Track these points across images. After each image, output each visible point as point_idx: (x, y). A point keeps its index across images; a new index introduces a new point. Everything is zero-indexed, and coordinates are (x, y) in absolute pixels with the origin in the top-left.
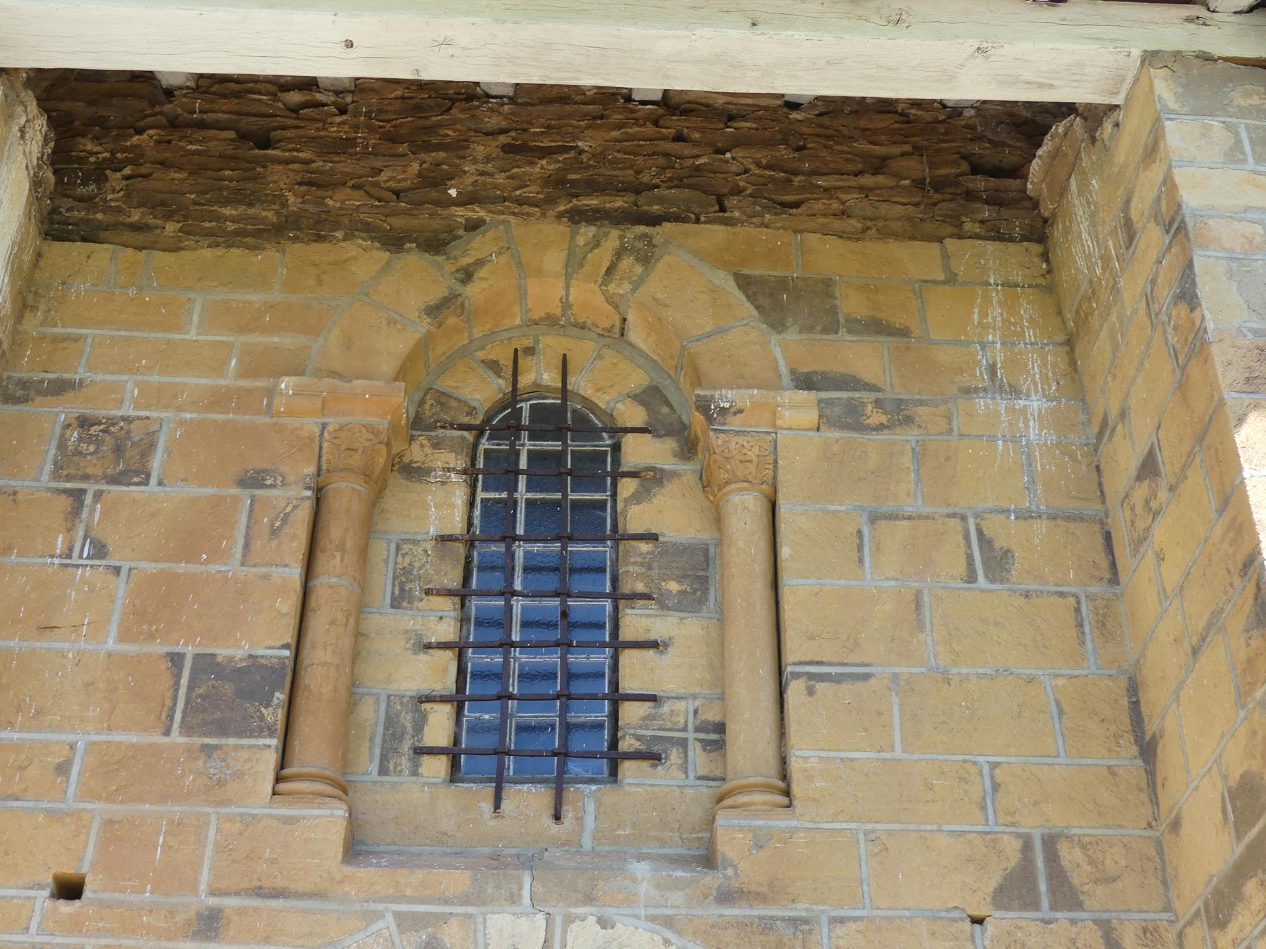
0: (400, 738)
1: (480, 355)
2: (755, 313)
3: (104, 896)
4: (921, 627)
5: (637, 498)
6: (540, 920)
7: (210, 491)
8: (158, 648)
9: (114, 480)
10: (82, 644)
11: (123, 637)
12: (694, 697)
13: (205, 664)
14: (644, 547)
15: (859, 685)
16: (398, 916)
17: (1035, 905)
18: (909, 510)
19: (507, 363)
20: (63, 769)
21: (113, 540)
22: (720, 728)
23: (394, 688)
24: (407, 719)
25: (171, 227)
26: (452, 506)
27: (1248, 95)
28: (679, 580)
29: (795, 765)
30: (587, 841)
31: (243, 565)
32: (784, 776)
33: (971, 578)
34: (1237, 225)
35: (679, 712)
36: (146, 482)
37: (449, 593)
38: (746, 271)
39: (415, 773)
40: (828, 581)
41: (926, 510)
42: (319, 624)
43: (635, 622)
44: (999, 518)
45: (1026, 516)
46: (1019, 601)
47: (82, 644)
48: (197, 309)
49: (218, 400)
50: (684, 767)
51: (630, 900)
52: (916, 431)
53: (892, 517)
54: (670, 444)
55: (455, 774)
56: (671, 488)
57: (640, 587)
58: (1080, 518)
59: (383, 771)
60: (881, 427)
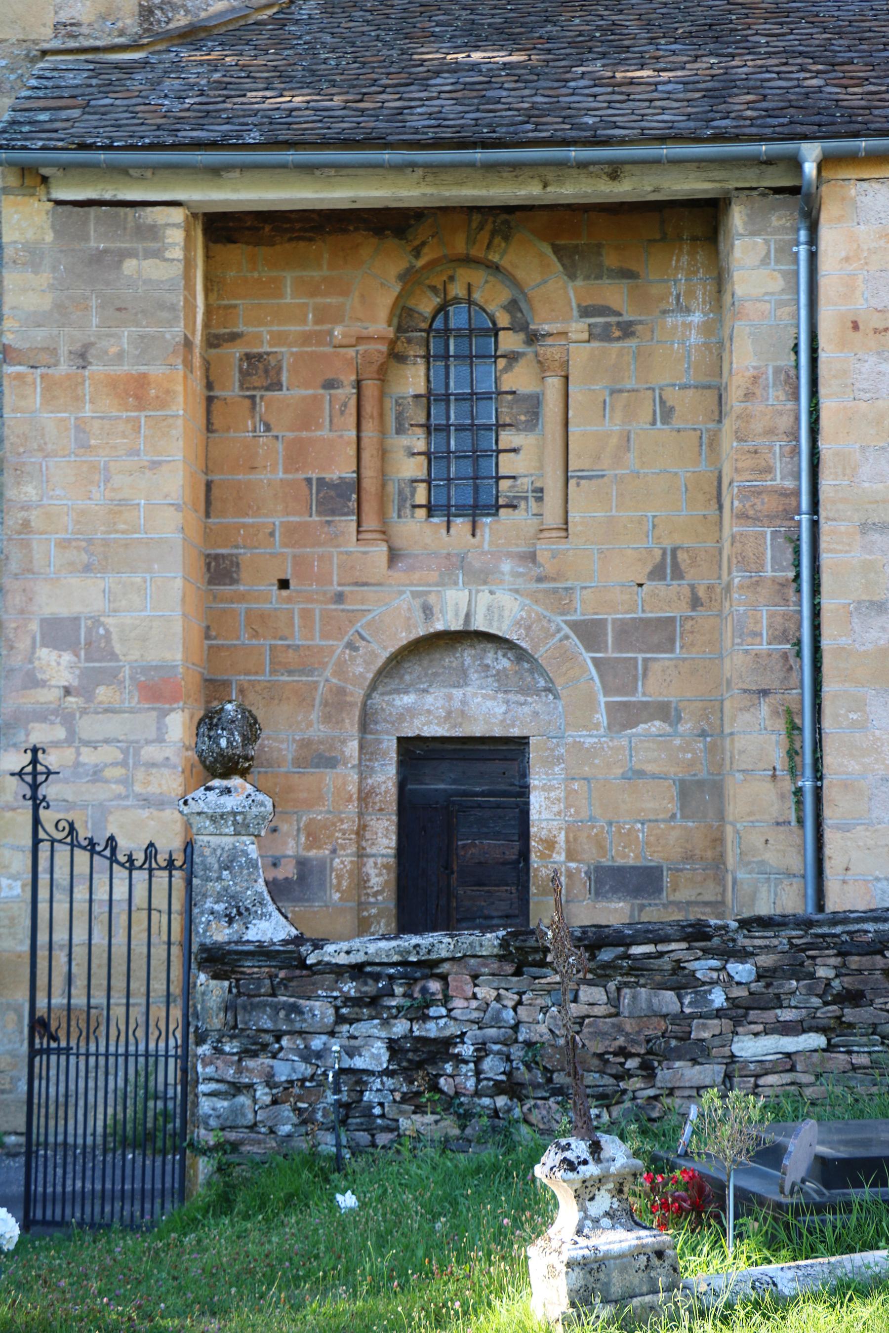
0: (405, 501)
1: (427, 282)
2: (561, 269)
3: (299, 588)
4: (629, 450)
5: (506, 369)
6: (467, 592)
7: (310, 392)
8: (301, 476)
9: (267, 389)
10: (269, 476)
11: (286, 471)
12: (532, 475)
13: (320, 481)
14: (510, 397)
15: (600, 481)
16: (412, 592)
17: (664, 579)
18: (629, 387)
19: (440, 287)
20: (272, 534)
21: (272, 422)
22: (541, 490)
23: (400, 476)
24: (407, 491)
25: (267, 228)
26: (419, 376)
27: (780, 218)
28: (525, 414)
29: (570, 519)
30: (486, 547)
31: (331, 430)
32: (566, 523)
33: (654, 423)
34: (758, 305)
35: (525, 483)
36: (281, 389)
37: (421, 426)
38: (558, 242)
39: (413, 517)
40: (588, 428)
41: (636, 387)
42: (366, 455)
43: (507, 438)
44: (670, 389)
45: (684, 387)
46: (674, 433)
47: (269, 476)
48: (289, 283)
49: (307, 339)
50: (527, 510)
51: (502, 582)
52: (636, 340)
53: (621, 391)
54: (522, 336)
55: (430, 515)
56: (522, 362)
57: (508, 421)
58: (709, 387)
59: (399, 516)
60: (619, 339)
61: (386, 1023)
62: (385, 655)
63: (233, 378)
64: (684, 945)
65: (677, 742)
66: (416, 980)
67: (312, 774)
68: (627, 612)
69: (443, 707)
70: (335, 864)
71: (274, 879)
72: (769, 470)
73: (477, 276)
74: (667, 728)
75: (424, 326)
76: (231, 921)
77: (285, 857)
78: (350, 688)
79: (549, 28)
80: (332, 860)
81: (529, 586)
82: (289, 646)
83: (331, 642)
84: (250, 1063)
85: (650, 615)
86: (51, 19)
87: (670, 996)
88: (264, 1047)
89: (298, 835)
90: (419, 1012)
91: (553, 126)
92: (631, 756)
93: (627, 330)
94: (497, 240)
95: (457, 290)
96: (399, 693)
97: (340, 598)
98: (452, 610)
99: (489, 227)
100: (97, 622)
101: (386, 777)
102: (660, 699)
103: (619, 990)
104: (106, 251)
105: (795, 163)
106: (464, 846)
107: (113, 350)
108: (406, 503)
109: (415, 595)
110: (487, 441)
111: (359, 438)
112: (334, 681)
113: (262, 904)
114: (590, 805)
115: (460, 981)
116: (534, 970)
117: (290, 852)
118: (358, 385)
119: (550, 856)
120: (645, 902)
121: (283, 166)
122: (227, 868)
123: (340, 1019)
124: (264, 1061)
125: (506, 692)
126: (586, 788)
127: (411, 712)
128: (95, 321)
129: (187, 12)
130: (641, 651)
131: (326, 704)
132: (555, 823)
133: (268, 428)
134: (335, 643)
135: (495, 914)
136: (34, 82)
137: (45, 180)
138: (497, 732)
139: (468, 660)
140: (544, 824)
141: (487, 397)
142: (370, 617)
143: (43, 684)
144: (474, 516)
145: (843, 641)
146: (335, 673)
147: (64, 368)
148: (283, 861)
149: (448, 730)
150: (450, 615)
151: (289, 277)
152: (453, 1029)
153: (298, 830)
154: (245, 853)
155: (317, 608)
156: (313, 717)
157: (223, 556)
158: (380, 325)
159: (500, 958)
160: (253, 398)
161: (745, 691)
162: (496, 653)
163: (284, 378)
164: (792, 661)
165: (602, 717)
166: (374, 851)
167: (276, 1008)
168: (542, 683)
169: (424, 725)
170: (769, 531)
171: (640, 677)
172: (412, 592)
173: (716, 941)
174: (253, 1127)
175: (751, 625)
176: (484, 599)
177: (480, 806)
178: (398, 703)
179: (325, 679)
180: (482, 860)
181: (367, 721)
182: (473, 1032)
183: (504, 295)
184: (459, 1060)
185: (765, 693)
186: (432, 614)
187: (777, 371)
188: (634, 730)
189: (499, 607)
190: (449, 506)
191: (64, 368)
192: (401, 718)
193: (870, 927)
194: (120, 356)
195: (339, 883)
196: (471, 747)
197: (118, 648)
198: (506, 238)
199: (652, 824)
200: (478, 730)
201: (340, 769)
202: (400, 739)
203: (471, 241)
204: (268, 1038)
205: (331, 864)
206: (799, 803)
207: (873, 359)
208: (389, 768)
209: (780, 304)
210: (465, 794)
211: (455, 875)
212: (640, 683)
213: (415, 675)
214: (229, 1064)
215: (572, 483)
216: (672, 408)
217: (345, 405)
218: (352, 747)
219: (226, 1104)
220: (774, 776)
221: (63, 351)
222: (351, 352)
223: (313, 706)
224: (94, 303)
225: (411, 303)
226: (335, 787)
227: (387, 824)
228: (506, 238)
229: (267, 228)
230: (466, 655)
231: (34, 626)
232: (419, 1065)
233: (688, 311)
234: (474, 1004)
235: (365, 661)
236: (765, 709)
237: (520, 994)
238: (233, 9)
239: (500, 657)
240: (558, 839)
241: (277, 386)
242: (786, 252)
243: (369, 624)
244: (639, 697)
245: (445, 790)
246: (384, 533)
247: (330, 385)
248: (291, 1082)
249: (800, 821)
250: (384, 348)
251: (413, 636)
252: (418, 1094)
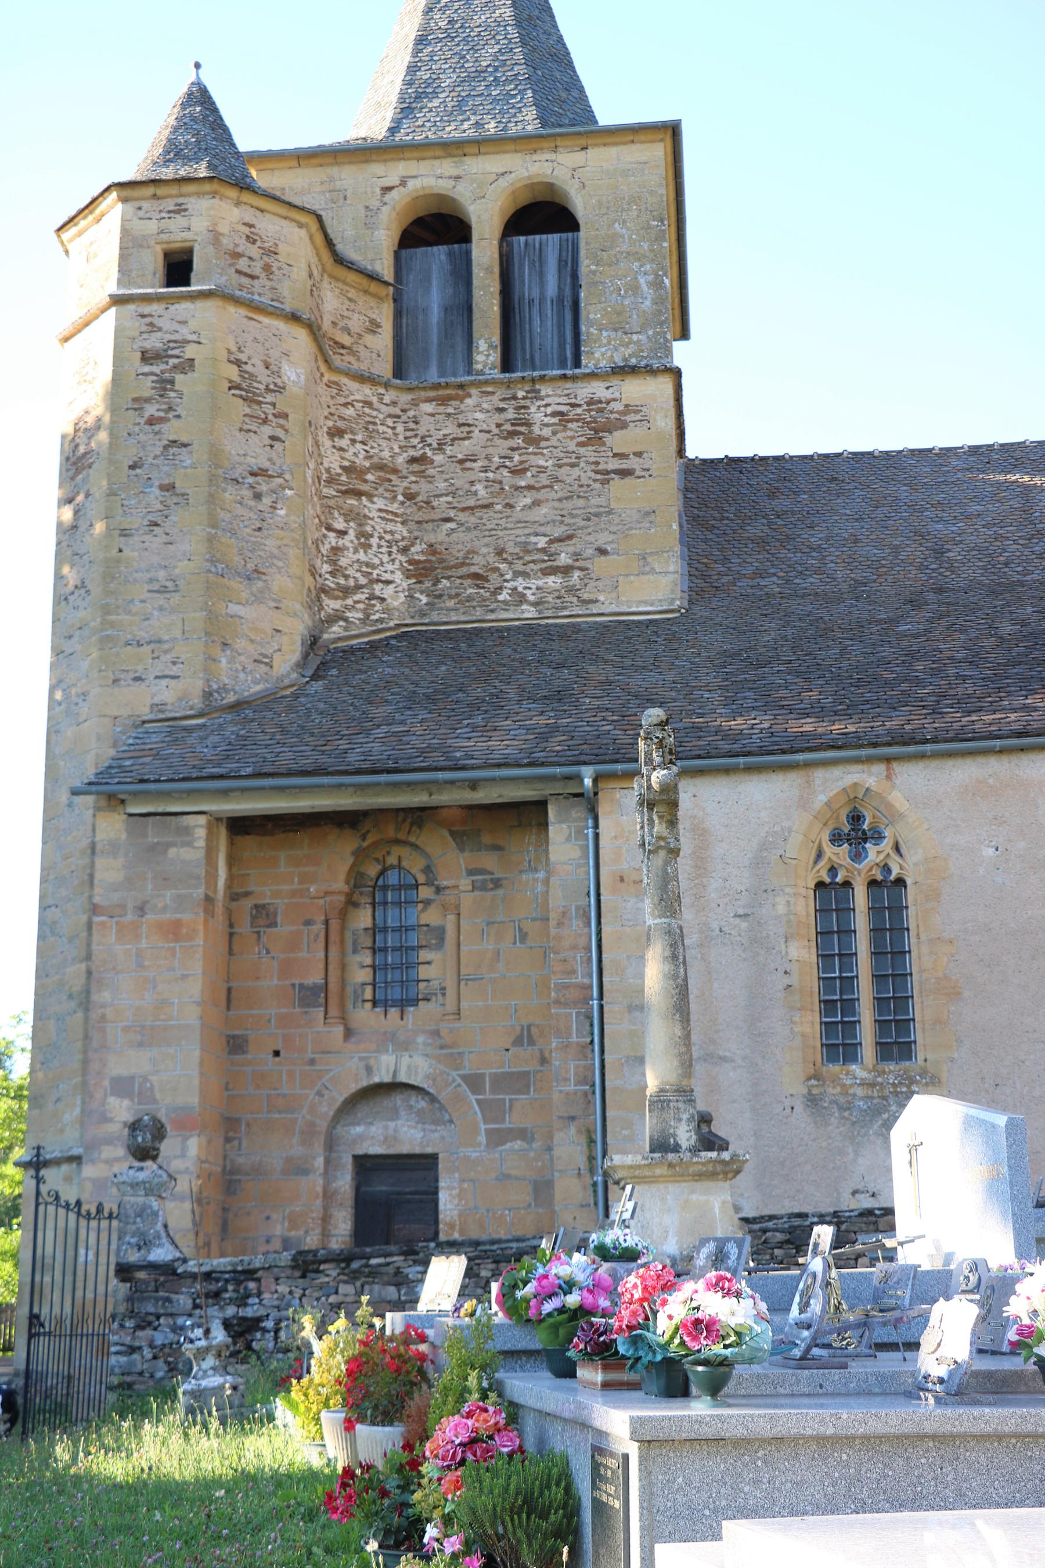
5: (423, 911)
8: (288, 982)
9: (268, 926)
13: (301, 986)
17: (522, 1045)
20: (269, 1021)
35: (435, 984)
42: (331, 968)
43: (424, 955)
45: (534, 920)
49: (293, 894)
53: (493, 923)
56: (433, 905)
61: (222, 1308)
62: (341, 1099)
63: (242, 920)
64: (402, 1258)
65: (532, 1154)
66: (242, 1282)
72: (574, 972)
73: (405, 851)
74: (526, 1146)
75: (371, 883)
76: (139, 1249)
78: (318, 1121)
79: (460, 695)
84: (140, 1334)
86: (149, 702)
87: (392, 1289)
88: (150, 1324)
90: (242, 1301)
91: (439, 760)
93: (497, 884)
94: (414, 828)
95: (392, 860)
97: (312, 1062)
98: (386, 1067)
99: (409, 820)
100: (145, 1079)
101: (345, 1182)
103: (362, 1286)
104: (158, 843)
105: (578, 778)
107: (160, 905)
108: (358, 999)
109: (361, 1059)
110: (413, 956)
111: (327, 957)
113: (159, 1238)
115: (268, 1281)
116: (313, 1275)
117: (278, 1233)
118: (327, 922)
121: (262, 788)
122: (139, 1216)
123: (196, 1306)
124: (149, 1332)
127: (361, 1137)
128: (150, 887)
129: (235, 693)
133: (268, 952)
136: (131, 741)
137: (123, 802)
138: (417, 1150)
139: (399, 1103)
141: (412, 928)
143: (110, 1120)
144: (402, 1006)
145: (619, 1083)
147: (130, 917)
150: (383, 1072)
151: (282, 855)
152: (262, 1312)
154: (150, 1207)
156: (294, 1141)
157: (238, 1036)
158: (340, 884)
159: (293, 1268)
160: (258, 933)
161: (560, 1117)
163: (279, 919)
164: (590, 1097)
165: (482, 1139)
166: (336, 1232)
167: (157, 1300)
168: (447, 1117)
170: (574, 1012)
173: (421, 1255)
174: (141, 1374)
175: (567, 1071)
176: (405, 1060)
177: (409, 1201)
178: (353, 1132)
181: (331, 1144)
182: (274, 1314)
183: (422, 863)
184: (265, 1330)
185: (573, 1118)
187: (578, 908)
189: (414, 1066)
190: (386, 1000)
191: (130, 917)
192: (354, 1142)
193: (514, 1245)
194: (165, 908)
197: (158, 1096)
198: (420, 827)
200: (404, 1149)
201: (311, 1176)
202: (356, 1157)
203: (398, 829)
204: (151, 1318)
206: (595, 1191)
207: (634, 900)
209: (578, 866)
210: (399, 1193)
214: (128, 1334)
215: (463, 983)
216: (526, 934)
217: (317, 936)
218: (320, 1162)
219: (125, 1359)
220: (579, 1174)
221: (130, 906)
222: (321, 902)
224: (149, 875)
225: (362, 869)
228: (420, 827)
229: (270, 825)
231: (106, 1083)
232: (241, 1334)
233: (536, 870)
234: (276, 1296)
236: (573, 1130)
237: (304, 1290)
238: (267, 689)
241: (274, 924)
242: (580, 833)
246: (343, 1019)
247: (308, 923)
248: (164, 1345)
249: (596, 1204)
250: (342, 898)
251: (359, 1087)
252: (239, 1352)
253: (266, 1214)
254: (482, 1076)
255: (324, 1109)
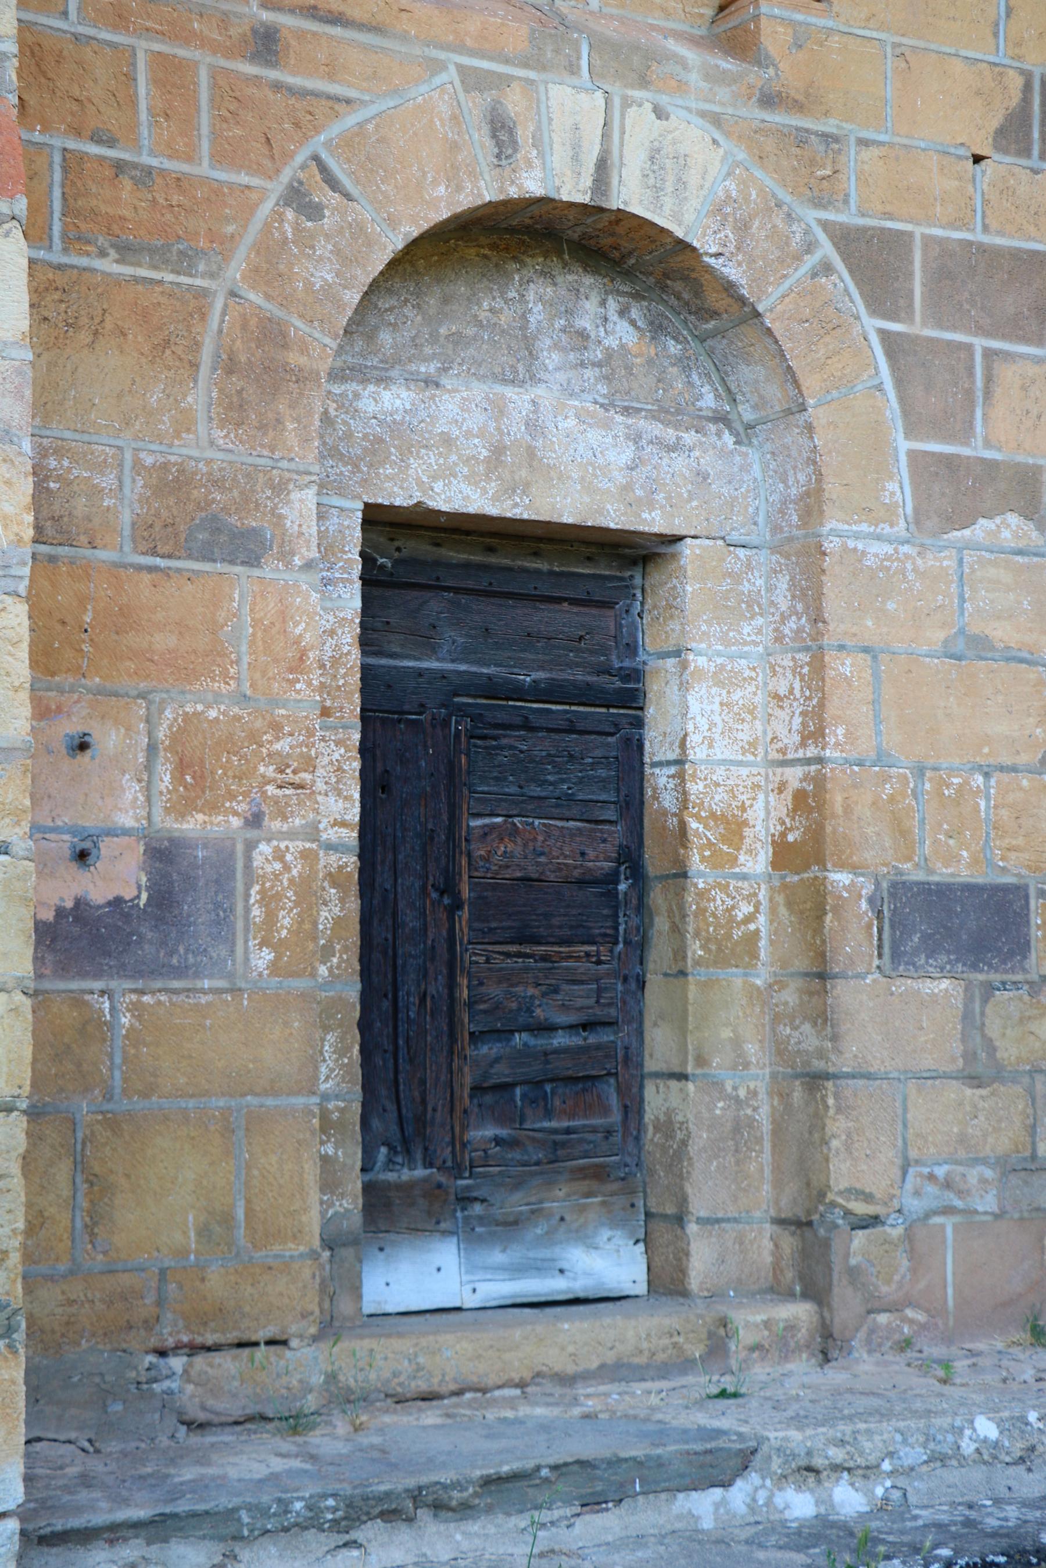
17: (1025, 151)
67: (192, 577)
68: (951, 225)
69: (482, 434)
70: (258, 861)
71: (80, 903)
77: (112, 832)
80: (250, 846)
81: (743, 112)
82: (120, 167)
83: (244, 179)
85: (999, 241)
89: (149, 767)
92: (962, 599)
96: (365, 381)
102: (1020, 458)
106: (487, 832)
112: (255, 297)
114: (878, 719)
117: (127, 820)
119: (734, 861)
120: (995, 977)
125: (627, 411)
126: (867, 674)
130: (981, 331)
131: (230, 366)
132: (744, 771)
134: (255, 181)
135: (562, 1019)
140: (719, 774)
142: (351, 120)
146: (256, 275)
148: (107, 847)
149: (495, 499)
153: (152, 749)
155: (204, 62)
162: (603, 303)
165: (899, 490)
169: (434, 478)
171: (979, 394)
172: (461, 68)
178: (366, 406)
179: (229, 285)
180: (533, 872)
186: (514, 143)
188: (967, 532)
195: (271, 919)
196: (507, 562)
199: (1005, 777)
201: (270, 570)
205: (248, 859)
208: (341, 589)
210: (491, 689)
211: (465, 913)
212: (979, 413)
213: (407, 333)
223: (195, 366)
226: (256, 623)
227: (338, 753)
230: (531, 296)
235: (337, 252)
239: (614, 317)
240: (749, 815)
243: (348, 143)
244: (974, 450)
245: (443, 676)
251: (465, 201)
253: (72, 727)
254: (899, 242)
255: (324, 275)
